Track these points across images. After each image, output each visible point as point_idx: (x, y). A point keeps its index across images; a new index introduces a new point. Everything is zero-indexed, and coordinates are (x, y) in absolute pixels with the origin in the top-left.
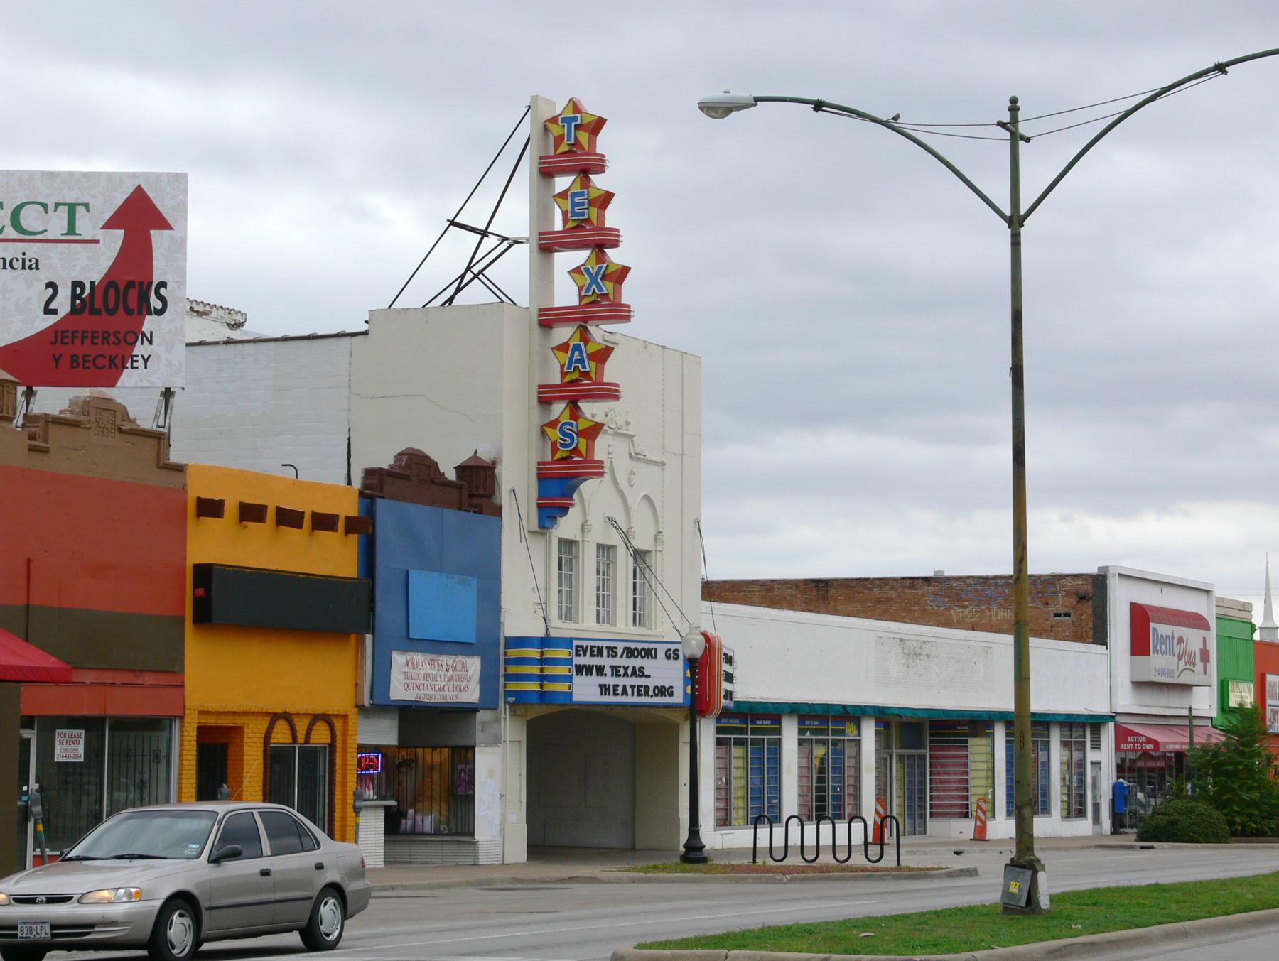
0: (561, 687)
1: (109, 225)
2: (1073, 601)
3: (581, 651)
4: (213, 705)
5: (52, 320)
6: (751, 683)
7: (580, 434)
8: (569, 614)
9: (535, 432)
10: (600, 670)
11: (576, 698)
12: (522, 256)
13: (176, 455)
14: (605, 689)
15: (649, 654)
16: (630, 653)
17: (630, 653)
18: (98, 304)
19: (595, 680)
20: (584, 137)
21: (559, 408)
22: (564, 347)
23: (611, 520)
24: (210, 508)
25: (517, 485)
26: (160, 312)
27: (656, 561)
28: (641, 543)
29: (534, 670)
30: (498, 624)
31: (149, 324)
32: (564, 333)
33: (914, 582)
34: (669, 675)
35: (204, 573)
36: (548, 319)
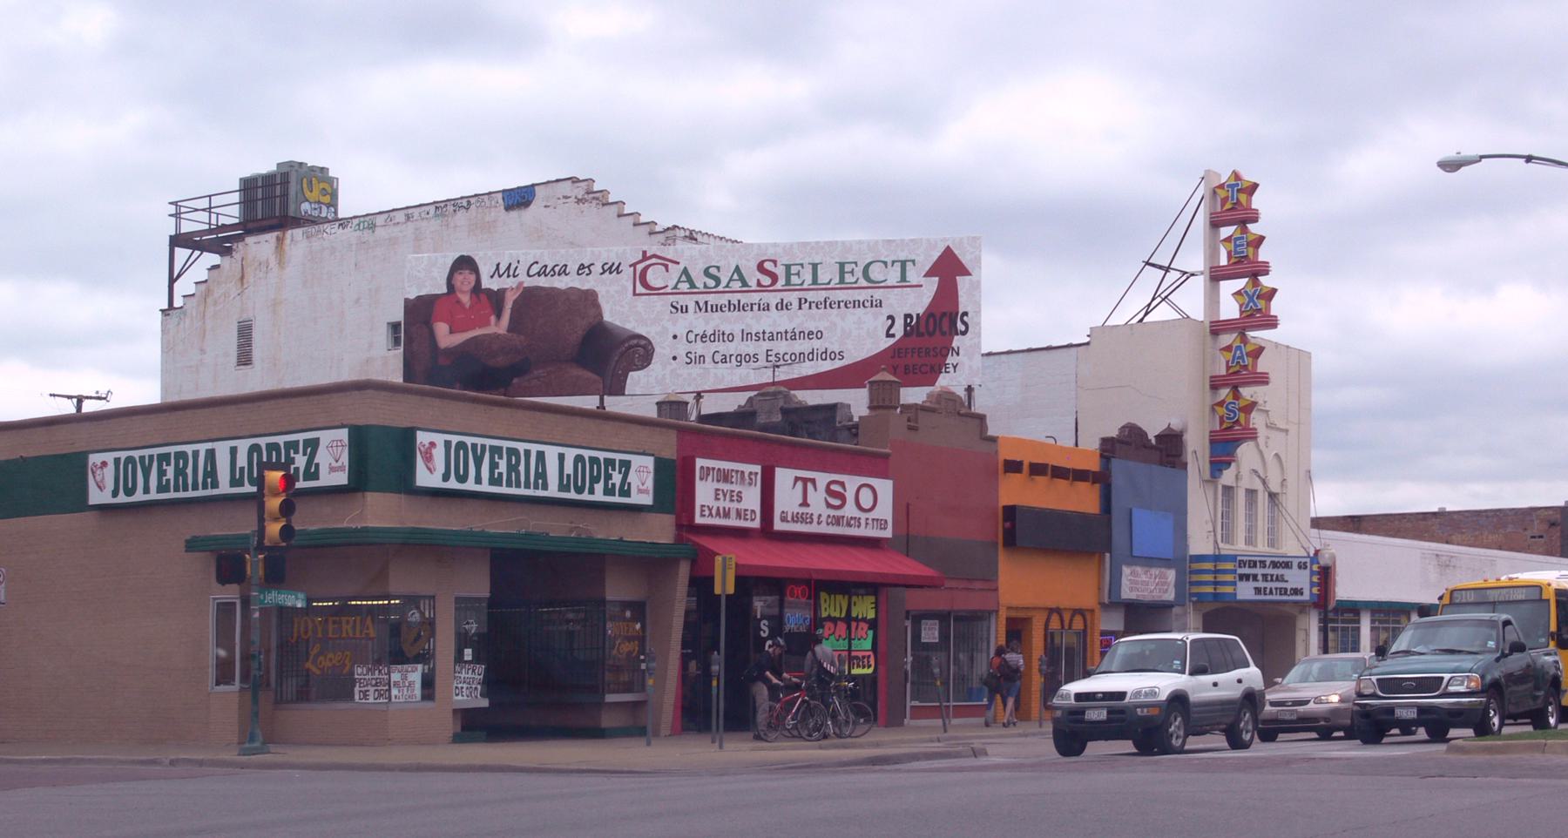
0: (1229, 589)
1: (929, 274)
2: (1546, 526)
3: (1242, 564)
4: (1015, 603)
5: (891, 341)
6: (1346, 589)
7: (1240, 409)
8: (1228, 538)
9: (1207, 409)
10: (1255, 577)
11: (1239, 597)
12: (1198, 285)
13: (992, 431)
14: (1258, 591)
15: (1287, 565)
16: (1275, 565)
17: (1275, 565)
18: (922, 330)
19: (1252, 584)
20: (1243, 198)
21: (1224, 393)
22: (1228, 348)
23: (1255, 472)
24: (1013, 467)
25: (1196, 446)
26: (964, 333)
27: (1282, 499)
28: (1275, 488)
29: (1209, 578)
30: (1186, 547)
31: (957, 341)
32: (1227, 339)
33: (1425, 516)
34: (1300, 579)
35: (1010, 512)
36: (1217, 328)
